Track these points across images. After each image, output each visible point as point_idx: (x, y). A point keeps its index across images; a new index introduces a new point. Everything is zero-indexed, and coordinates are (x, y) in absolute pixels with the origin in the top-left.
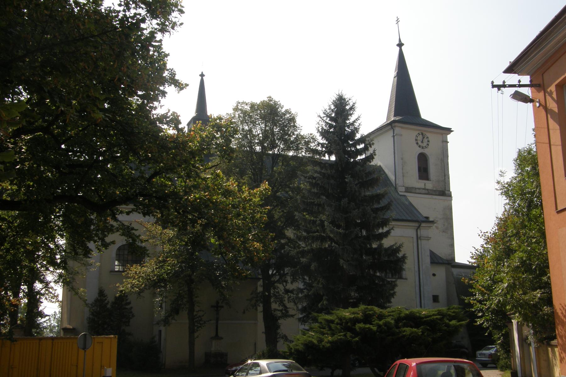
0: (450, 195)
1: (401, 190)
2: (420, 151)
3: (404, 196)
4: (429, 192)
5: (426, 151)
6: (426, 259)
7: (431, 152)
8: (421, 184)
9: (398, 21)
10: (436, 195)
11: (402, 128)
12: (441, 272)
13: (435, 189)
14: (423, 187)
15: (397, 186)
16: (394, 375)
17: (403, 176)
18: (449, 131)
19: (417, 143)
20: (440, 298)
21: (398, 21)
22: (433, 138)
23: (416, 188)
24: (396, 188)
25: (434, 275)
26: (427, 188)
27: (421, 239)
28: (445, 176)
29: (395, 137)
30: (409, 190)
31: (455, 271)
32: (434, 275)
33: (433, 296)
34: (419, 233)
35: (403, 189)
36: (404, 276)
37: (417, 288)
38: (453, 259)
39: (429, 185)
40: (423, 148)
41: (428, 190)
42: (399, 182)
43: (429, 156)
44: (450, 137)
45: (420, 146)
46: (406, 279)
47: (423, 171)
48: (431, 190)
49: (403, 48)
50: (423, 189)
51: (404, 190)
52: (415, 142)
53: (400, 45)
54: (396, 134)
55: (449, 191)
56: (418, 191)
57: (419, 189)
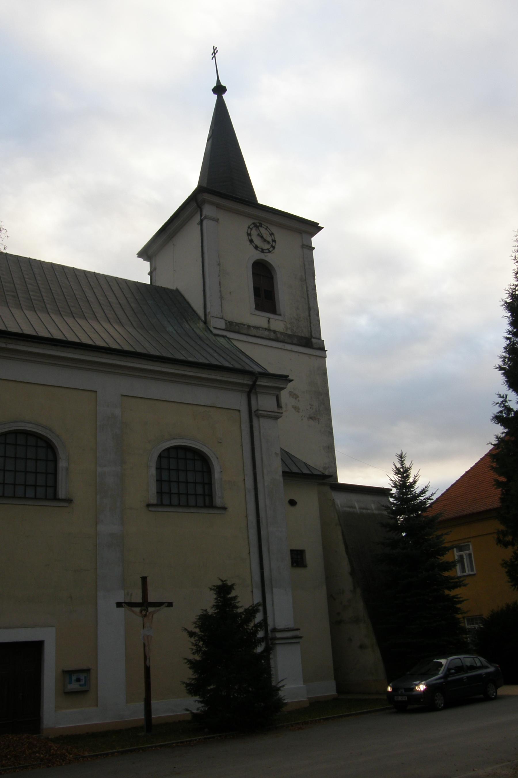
0: (322, 349)
1: (216, 323)
2: (258, 256)
3: (224, 337)
4: (276, 337)
5: (269, 258)
6: (272, 469)
7: (280, 259)
8: (260, 319)
9: (214, 53)
10: (292, 344)
11: (218, 206)
12: (309, 499)
13: (289, 332)
14: (266, 325)
15: (209, 317)
16: (3, 345)
17: (221, 298)
18: (314, 228)
19: (251, 241)
20: (309, 557)
21: (214, 53)
22: (285, 241)
23: (249, 327)
24: (205, 322)
25: (292, 503)
26: (272, 327)
27: (258, 416)
28: (309, 309)
29: (205, 223)
30: (233, 327)
31: (340, 499)
32: (292, 503)
33: (292, 551)
34: (253, 402)
35: (223, 325)
36: (218, 502)
37: (253, 532)
38: (334, 476)
39: (278, 325)
40: (262, 251)
41: (275, 332)
42: (213, 309)
43: (276, 269)
44: (316, 240)
45: (256, 247)
46: (224, 508)
47: (265, 297)
48: (282, 333)
49: (225, 97)
50: (266, 329)
51: (223, 327)
52: (246, 238)
53: (219, 90)
54: (205, 218)
55: (320, 338)
56: (253, 332)
57: (257, 328)
